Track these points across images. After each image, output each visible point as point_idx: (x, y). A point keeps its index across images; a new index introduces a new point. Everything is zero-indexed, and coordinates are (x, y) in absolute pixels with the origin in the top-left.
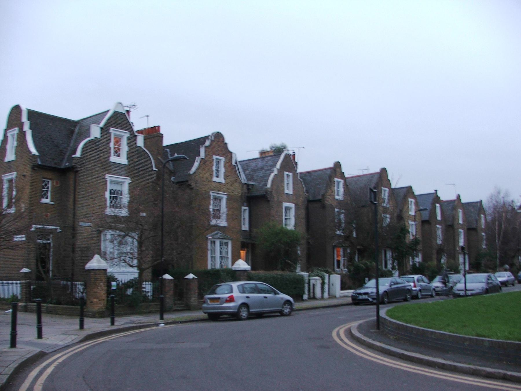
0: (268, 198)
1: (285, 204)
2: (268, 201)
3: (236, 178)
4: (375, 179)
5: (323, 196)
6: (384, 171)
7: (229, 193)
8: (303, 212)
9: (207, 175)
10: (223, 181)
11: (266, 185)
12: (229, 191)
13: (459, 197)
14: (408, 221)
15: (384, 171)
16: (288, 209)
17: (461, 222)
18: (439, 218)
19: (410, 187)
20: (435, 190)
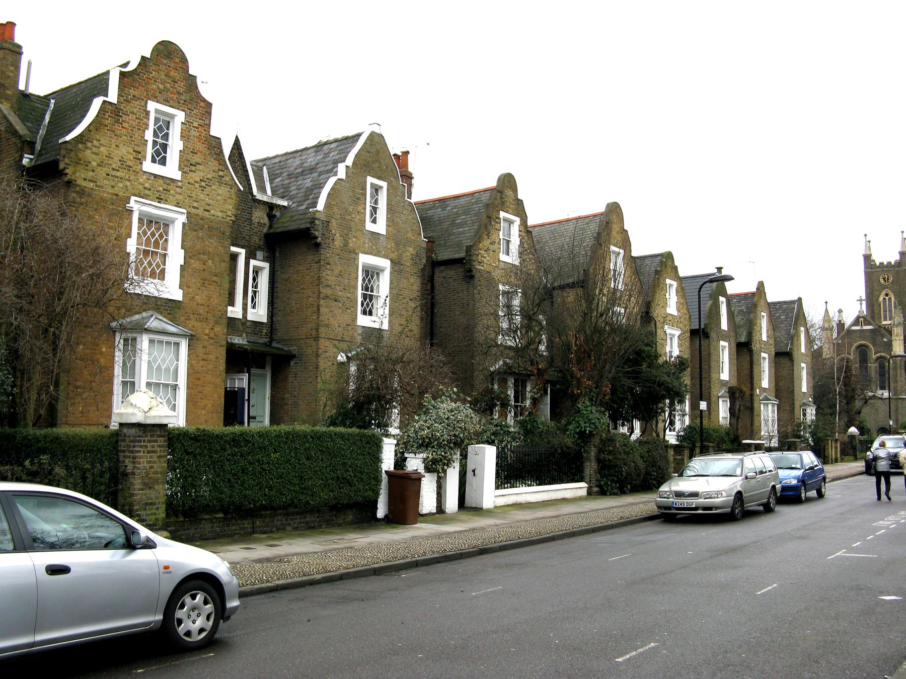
0: (316, 238)
1: (365, 259)
2: (317, 245)
3: (221, 173)
4: (594, 227)
5: (469, 249)
6: (614, 210)
7: (193, 211)
8: (413, 285)
9: (125, 151)
10: (177, 175)
11: (315, 204)
12: (195, 204)
13: (761, 286)
14: (663, 328)
15: (614, 210)
16: (371, 273)
17: (764, 338)
18: (724, 325)
19: (669, 256)
20: (717, 268)
